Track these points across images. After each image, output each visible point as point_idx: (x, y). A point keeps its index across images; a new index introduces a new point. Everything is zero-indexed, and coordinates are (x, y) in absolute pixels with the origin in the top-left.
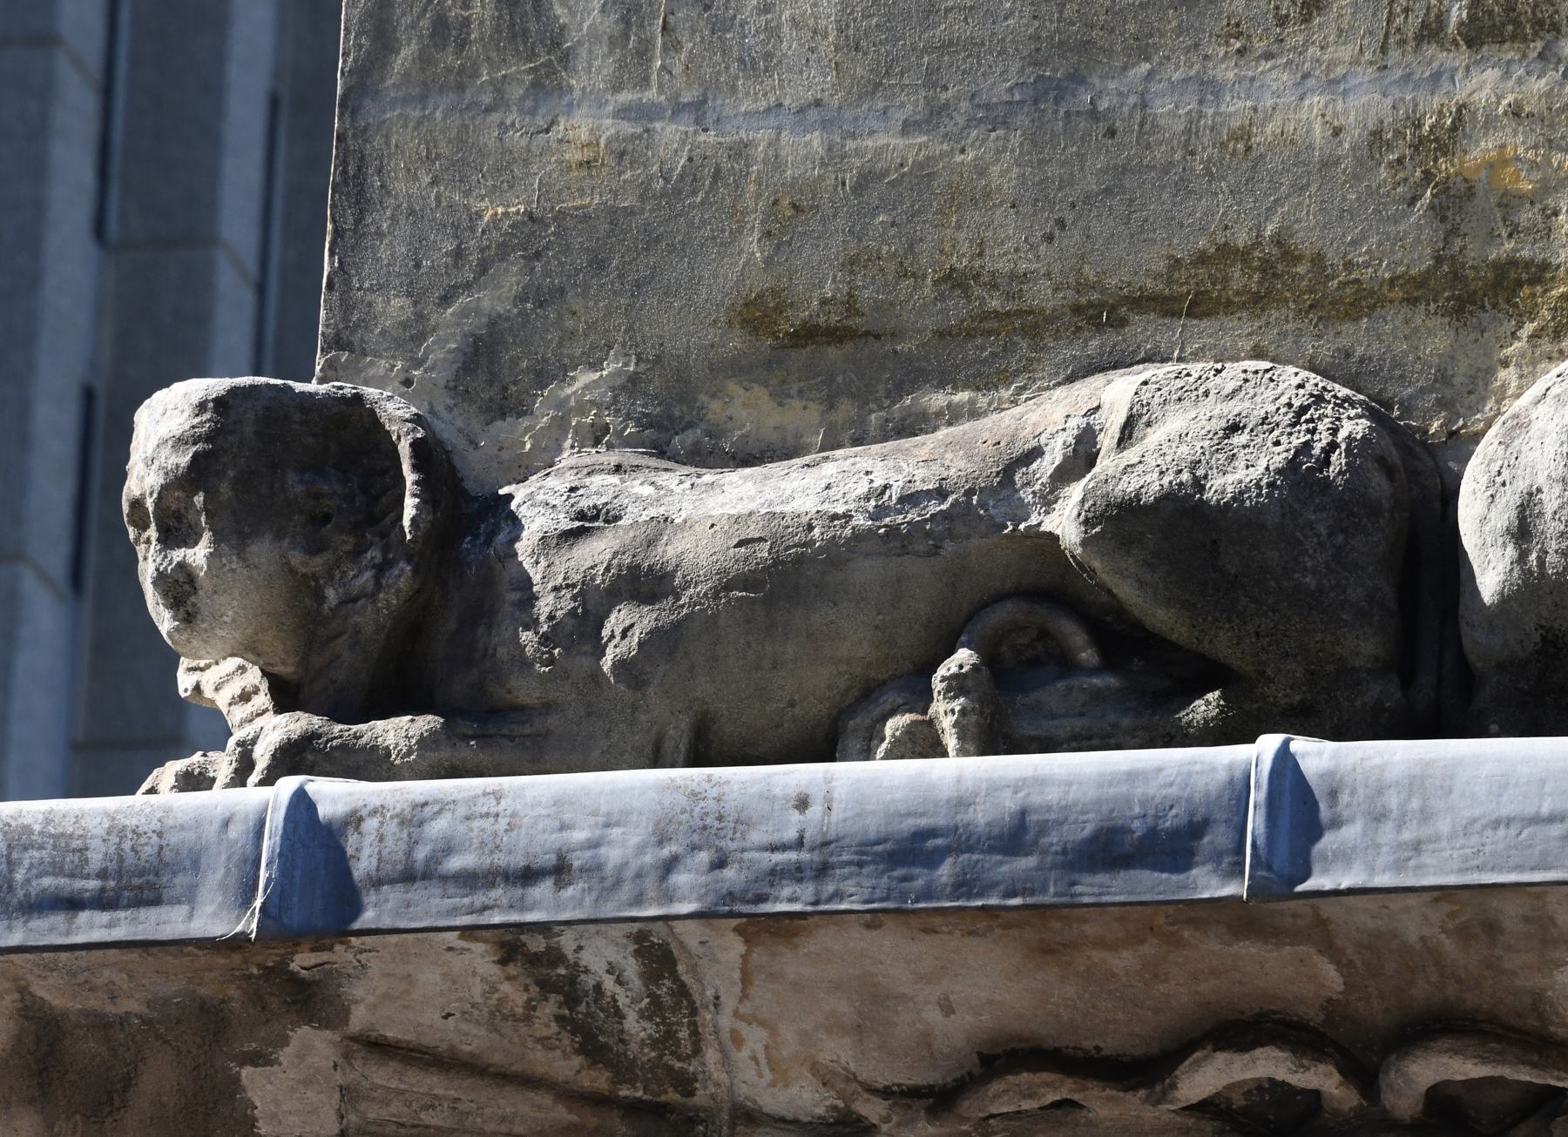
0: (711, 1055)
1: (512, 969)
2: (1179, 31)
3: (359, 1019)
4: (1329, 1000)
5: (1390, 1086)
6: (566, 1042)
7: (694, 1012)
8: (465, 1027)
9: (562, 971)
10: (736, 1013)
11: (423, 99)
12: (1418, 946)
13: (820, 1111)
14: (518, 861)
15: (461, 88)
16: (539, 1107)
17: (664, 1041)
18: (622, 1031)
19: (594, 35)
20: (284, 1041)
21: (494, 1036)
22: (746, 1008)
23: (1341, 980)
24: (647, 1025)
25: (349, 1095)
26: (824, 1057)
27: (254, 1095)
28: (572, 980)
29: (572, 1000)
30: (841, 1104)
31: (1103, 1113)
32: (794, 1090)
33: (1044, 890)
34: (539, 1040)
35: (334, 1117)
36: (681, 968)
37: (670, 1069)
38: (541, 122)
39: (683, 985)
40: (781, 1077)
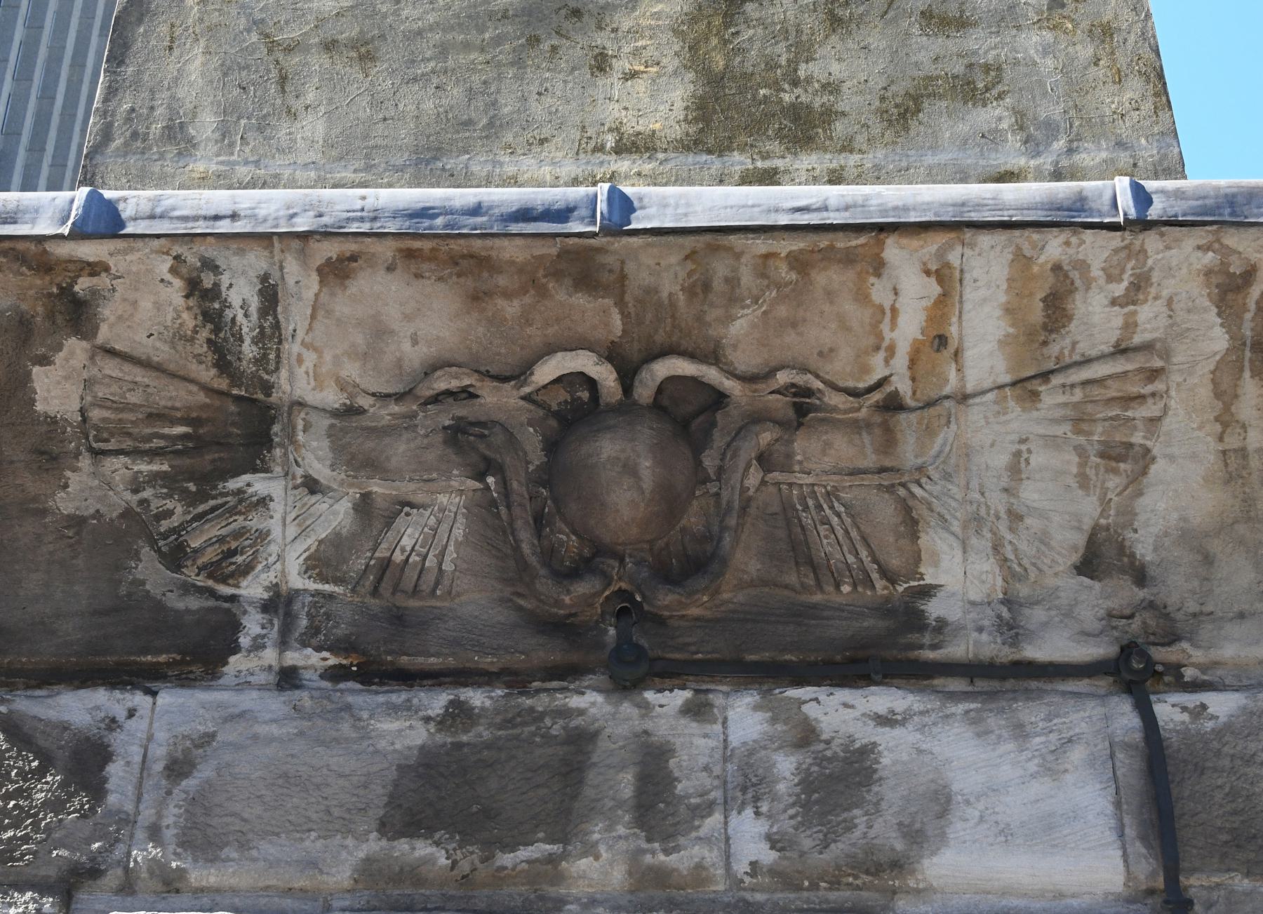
0: (284, 373)
1: (191, 302)
2: (483, 146)
3: (100, 339)
4: (612, 342)
5: (641, 382)
6: (210, 358)
7: (280, 342)
8: (158, 344)
9: (217, 306)
10: (303, 343)
11: (125, 155)
12: (666, 302)
13: (337, 406)
14: (213, 213)
15: (143, 153)
16: (190, 392)
17: (261, 361)
18: (240, 352)
19: (208, 139)
20: (59, 347)
21: (172, 351)
22: (308, 340)
23: (621, 328)
24: (254, 348)
25: (88, 384)
26: (344, 374)
27: (37, 385)
28: (220, 313)
29: (217, 330)
30: (348, 402)
31: (489, 400)
32: (325, 393)
33: (492, 228)
34: (195, 356)
35: (78, 400)
36: (279, 309)
37: (262, 378)
38: (181, 164)
39: (278, 322)
40: (320, 386)
